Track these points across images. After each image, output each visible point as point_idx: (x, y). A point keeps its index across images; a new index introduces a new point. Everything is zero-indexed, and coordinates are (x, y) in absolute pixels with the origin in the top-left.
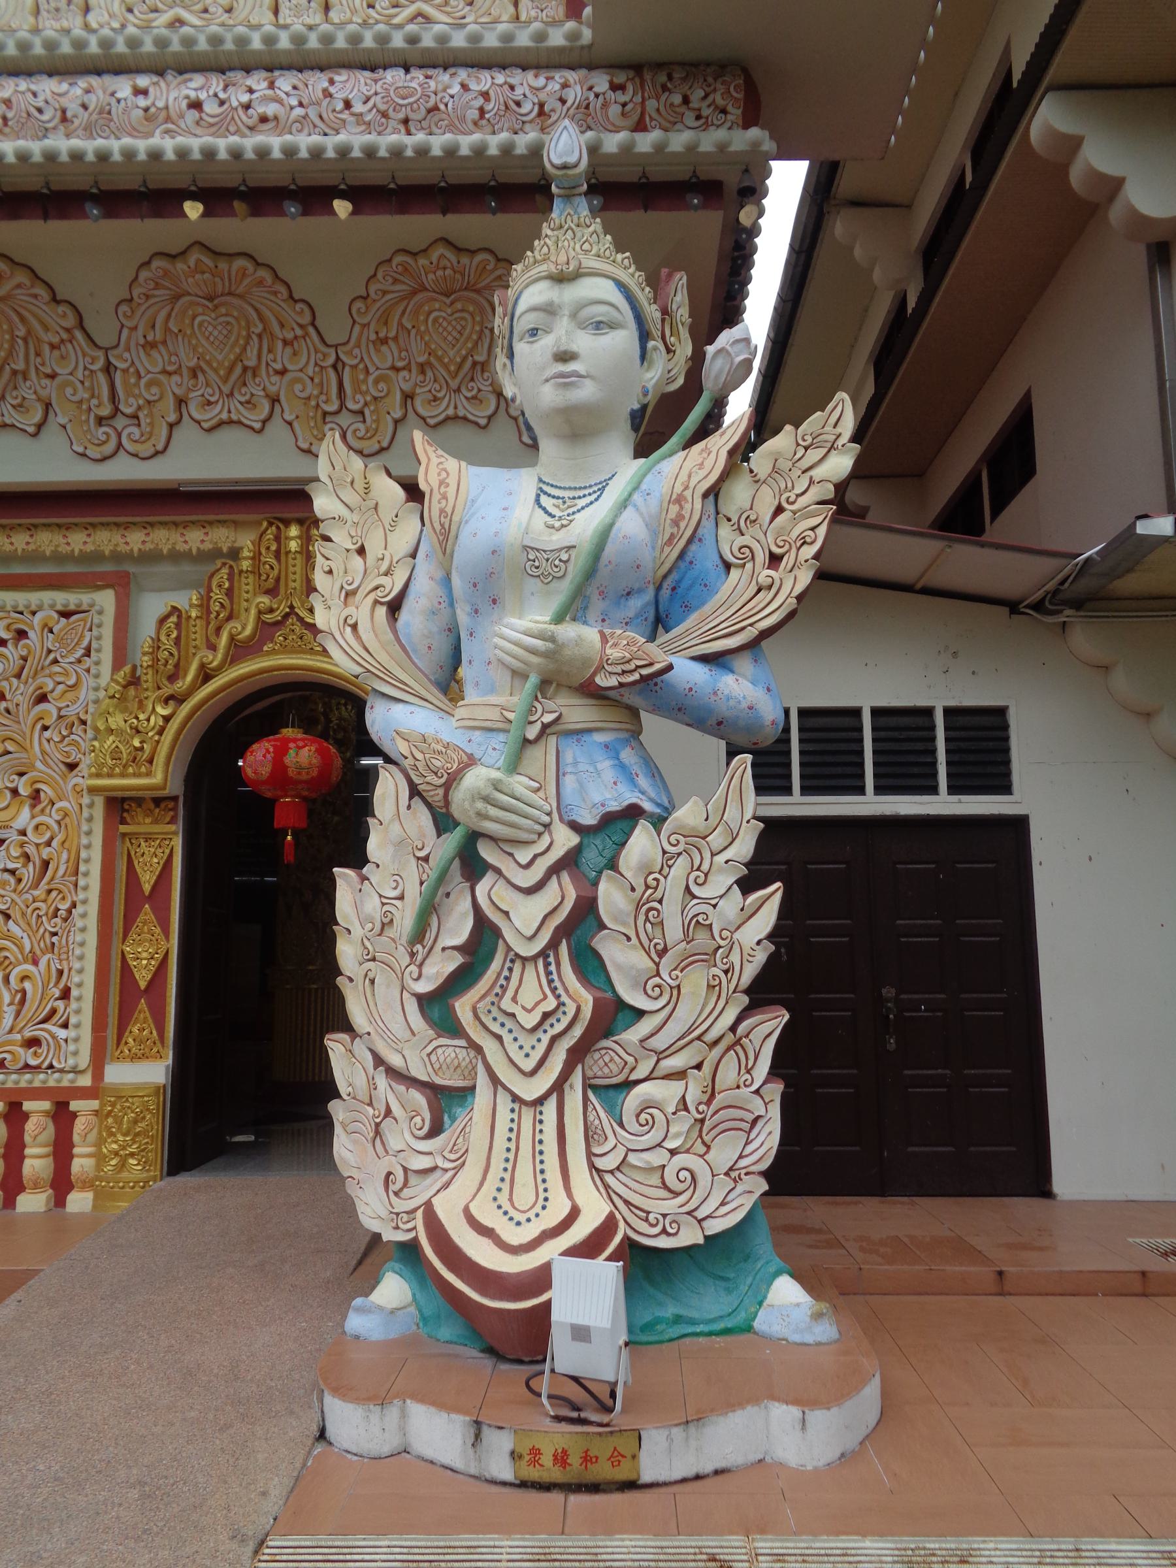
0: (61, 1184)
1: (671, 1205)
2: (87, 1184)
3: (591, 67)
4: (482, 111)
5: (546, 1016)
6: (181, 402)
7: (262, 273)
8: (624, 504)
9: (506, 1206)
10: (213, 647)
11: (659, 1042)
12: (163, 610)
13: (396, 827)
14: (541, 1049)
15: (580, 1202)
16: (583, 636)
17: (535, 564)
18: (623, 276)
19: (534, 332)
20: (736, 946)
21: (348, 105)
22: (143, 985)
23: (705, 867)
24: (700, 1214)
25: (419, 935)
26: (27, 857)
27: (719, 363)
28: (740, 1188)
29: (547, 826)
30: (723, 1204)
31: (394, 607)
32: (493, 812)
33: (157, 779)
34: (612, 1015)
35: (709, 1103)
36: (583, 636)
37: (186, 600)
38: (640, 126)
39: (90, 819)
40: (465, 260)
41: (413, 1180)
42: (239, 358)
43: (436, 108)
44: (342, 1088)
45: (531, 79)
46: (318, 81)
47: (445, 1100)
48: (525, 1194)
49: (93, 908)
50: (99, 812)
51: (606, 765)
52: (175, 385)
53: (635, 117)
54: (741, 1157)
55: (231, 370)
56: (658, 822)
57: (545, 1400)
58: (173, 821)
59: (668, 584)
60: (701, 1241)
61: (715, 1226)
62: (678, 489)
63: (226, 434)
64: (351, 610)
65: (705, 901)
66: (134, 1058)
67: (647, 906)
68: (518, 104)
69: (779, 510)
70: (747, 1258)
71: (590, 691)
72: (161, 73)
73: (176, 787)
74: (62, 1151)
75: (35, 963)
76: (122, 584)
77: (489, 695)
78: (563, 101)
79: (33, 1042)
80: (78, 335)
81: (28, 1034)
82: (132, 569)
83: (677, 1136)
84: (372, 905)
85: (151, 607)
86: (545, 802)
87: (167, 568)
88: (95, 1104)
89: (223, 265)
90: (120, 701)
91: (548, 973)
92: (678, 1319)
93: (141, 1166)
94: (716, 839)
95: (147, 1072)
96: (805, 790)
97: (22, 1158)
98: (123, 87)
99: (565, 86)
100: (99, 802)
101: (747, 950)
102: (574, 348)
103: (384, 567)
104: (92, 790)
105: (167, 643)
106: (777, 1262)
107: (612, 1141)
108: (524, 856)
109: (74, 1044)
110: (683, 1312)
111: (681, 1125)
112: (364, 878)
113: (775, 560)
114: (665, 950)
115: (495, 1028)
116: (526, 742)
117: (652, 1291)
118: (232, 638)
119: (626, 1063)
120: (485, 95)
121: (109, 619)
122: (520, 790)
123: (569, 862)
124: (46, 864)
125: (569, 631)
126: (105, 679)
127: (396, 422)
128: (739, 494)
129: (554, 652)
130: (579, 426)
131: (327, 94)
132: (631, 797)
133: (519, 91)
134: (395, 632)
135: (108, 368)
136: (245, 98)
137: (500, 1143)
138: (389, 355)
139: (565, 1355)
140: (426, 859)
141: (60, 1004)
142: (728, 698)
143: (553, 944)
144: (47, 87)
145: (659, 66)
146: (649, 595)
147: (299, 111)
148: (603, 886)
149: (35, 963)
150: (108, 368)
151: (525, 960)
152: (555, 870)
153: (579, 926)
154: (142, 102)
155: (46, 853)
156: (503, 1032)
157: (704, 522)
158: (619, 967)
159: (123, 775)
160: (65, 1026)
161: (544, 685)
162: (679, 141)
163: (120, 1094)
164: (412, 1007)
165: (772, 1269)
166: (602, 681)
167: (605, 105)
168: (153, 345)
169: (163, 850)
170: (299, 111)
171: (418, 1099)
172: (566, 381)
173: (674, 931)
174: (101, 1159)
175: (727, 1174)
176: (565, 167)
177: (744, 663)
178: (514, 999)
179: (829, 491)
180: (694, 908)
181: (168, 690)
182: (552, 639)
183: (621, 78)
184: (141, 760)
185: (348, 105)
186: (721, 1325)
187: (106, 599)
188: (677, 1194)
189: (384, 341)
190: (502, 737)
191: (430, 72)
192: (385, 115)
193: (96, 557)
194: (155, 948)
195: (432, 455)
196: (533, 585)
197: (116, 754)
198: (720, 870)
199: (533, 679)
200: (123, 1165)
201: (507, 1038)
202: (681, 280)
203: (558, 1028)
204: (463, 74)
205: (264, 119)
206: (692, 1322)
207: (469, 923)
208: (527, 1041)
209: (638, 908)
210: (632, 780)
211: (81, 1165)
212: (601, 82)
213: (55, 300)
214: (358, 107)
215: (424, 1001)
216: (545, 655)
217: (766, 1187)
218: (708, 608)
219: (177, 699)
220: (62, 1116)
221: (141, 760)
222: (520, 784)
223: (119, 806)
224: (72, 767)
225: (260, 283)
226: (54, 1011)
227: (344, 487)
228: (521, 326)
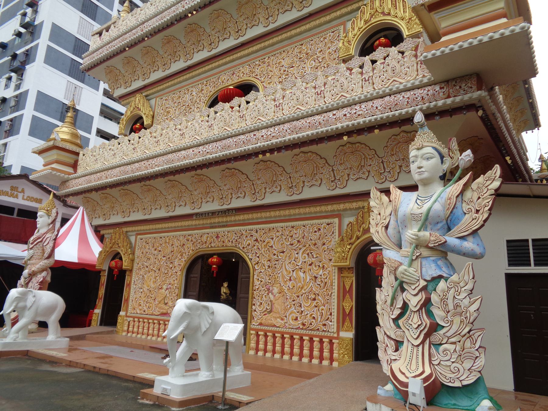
0: (332, 360)
1: (452, 376)
2: (337, 360)
3: (435, 84)
4: (408, 102)
5: (419, 325)
6: (349, 175)
7: (363, 146)
8: (435, 201)
9: (409, 369)
10: (359, 231)
11: (448, 334)
12: (348, 223)
13: (387, 279)
14: (418, 333)
15: (426, 370)
16: (425, 234)
17: (414, 217)
18: (434, 145)
19: (413, 162)
20: (468, 312)
21: (377, 108)
22: (347, 313)
23: (459, 291)
24: (461, 379)
25: (392, 305)
26: (322, 281)
27: (462, 162)
28: (472, 374)
29: (418, 280)
30: (467, 377)
31: (387, 227)
32: (405, 277)
33: (348, 263)
34: (434, 327)
35: (462, 351)
36: (425, 234)
37: (352, 219)
38: (449, 97)
39: (335, 272)
40: (409, 135)
41: (392, 361)
42: (360, 164)
43: (397, 104)
44: (379, 340)
45: (420, 91)
46: (370, 103)
47: (398, 344)
48: (414, 367)
49: (336, 294)
50: (336, 271)
51: (433, 266)
52: (347, 172)
53: (447, 95)
54: (472, 366)
55: (358, 167)
57: (407, 408)
58: (352, 273)
59: (449, 219)
60: (461, 386)
61: (465, 383)
62: (450, 196)
63: (359, 181)
64: (377, 228)
65: (459, 299)
66: (346, 331)
67: (444, 300)
68: (417, 98)
69: (479, 198)
70: (477, 394)
71: (427, 247)
72: (338, 109)
73: (353, 265)
74: (331, 351)
75: (324, 306)
76: (339, 216)
77: (407, 249)
78: (428, 95)
79: (325, 325)
80: (326, 164)
81: (323, 323)
82: (341, 213)
83: (454, 358)
84: (383, 297)
85: (346, 221)
86: (418, 274)
87: (349, 212)
88: (337, 341)
89: (354, 146)
90: (339, 245)
91: (420, 315)
92: (455, 405)
93: (348, 358)
94: (462, 284)
95: (349, 335)
96: (536, 265)
98: (330, 114)
99: (429, 91)
100: (336, 268)
101: (471, 313)
102: (422, 165)
103: (384, 217)
104: (335, 266)
105: (349, 231)
106: (486, 396)
107: (436, 357)
108: (413, 287)
109: (333, 326)
110: (457, 403)
111: (455, 356)
112: (381, 291)
113: (477, 211)
114: (449, 311)
115: (408, 327)
116: (413, 260)
117: (449, 397)
118: (363, 229)
120: (408, 98)
121: (337, 225)
122: (411, 271)
123: (424, 288)
124: (326, 283)
125: (422, 234)
126: (337, 239)
127: (398, 173)
128: (468, 194)
129: (418, 238)
130: (427, 182)
131: (372, 106)
132: (439, 273)
133: (417, 95)
134: (386, 233)
135: (333, 170)
136: (355, 111)
137: (409, 354)
138: (394, 158)
139: (411, 399)
140: (393, 287)
141: (330, 316)
142: (465, 248)
143: (421, 308)
144: (317, 117)
145: (453, 79)
146: (445, 222)
147: (366, 112)
148: (432, 295)
149: (324, 306)
150: (333, 170)
151: (414, 312)
152: (421, 290)
153: (427, 304)
154: (334, 117)
155: (326, 280)
156: (409, 328)
157: (457, 203)
158: (437, 315)
159: (340, 262)
160: (331, 322)
161: (417, 247)
162: (458, 99)
163: (343, 339)
164: (391, 321)
165: (483, 397)
166: (430, 245)
167: (439, 93)
168: (342, 164)
169: (351, 280)
170: (366, 112)
171: (393, 343)
172: (420, 173)
173: (451, 307)
174: (339, 354)
175: (468, 370)
176: (419, 122)
177: (470, 238)
178: (412, 321)
179: (493, 192)
180: (456, 301)
181: (350, 242)
182: (417, 236)
183: (443, 85)
184: (344, 259)
185: (377, 108)
186: (466, 408)
187: (336, 220)
188: (454, 373)
189: (393, 155)
190: (408, 259)
191: (395, 95)
192: (385, 108)
193: (334, 211)
195: (394, 191)
196: (414, 222)
198: (463, 292)
199: (414, 245)
200: (344, 356)
201: (410, 330)
202: (454, 140)
203: (422, 328)
204: (403, 94)
205: (359, 115)
206: (459, 406)
207: (402, 302)
208: (415, 331)
209: (441, 301)
210: (440, 268)
211: (335, 355)
212: (437, 88)
213: (321, 158)
214: (379, 108)
215: (393, 319)
216: (416, 239)
217: (124, 267)
218: (459, 225)
220: (331, 343)
221: (344, 259)
222: (411, 270)
223: (341, 270)
224: (331, 260)
225: (363, 148)
226: (328, 318)
227: (376, 200)
228: (411, 160)
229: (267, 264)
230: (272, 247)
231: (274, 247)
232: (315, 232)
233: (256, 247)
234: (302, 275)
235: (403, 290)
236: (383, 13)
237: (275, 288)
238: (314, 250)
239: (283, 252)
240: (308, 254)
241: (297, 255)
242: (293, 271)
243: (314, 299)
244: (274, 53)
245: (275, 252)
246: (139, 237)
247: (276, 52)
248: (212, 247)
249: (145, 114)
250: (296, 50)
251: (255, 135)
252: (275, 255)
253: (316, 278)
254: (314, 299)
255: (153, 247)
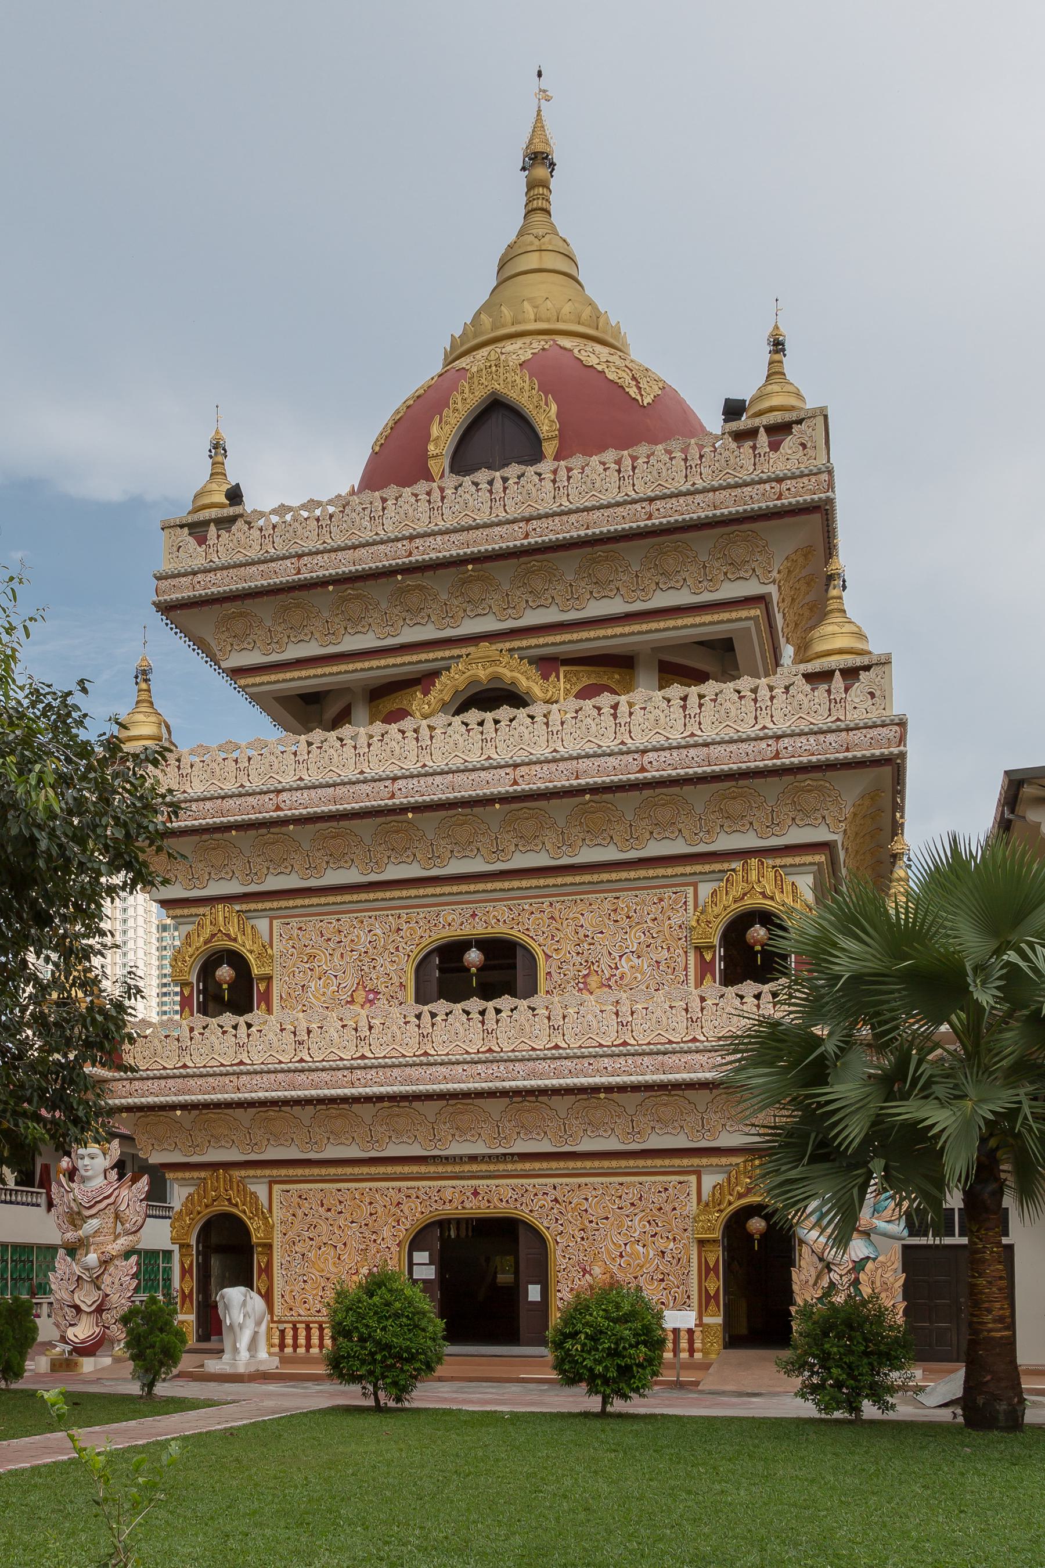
52: (722, 1121)
56: (874, 1260)
76: (698, 1174)
85: (709, 1181)
94: (889, 1264)
97: (679, 1343)
105: (717, 1195)
119: (761, 600)
169: (716, 1255)
187: (693, 1179)
194: (715, 1284)
197: (703, 1228)
211: (698, 1345)
219: (721, 1211)
223: (701, 1242)
224: (685, 1230)
229: (579, 1235)
230: (586, 1211)
231: (589, 1210)
232: (660, 1192)
233: (555, 1211)
234: (640, 1249)
235: (830, 1270)
236: (764, 895)
237: (596, 1268)
238: (658, 1217)
239: (607, 1218)
240: (649, 1222)
241: (630, 1223)
242: (626, 1244)
243: (662, 1280)
244: (562, 898)
245: (593, 1218)
246: (276, 1188)
247: (566, 898)
248: (464, 1208)
249: (251, 952)
250: (607, 905)
251: (590, 1064)
252: (591, 1222)
253: (663, 1253)
254: (662, 1280)
255: (322, 1205)
